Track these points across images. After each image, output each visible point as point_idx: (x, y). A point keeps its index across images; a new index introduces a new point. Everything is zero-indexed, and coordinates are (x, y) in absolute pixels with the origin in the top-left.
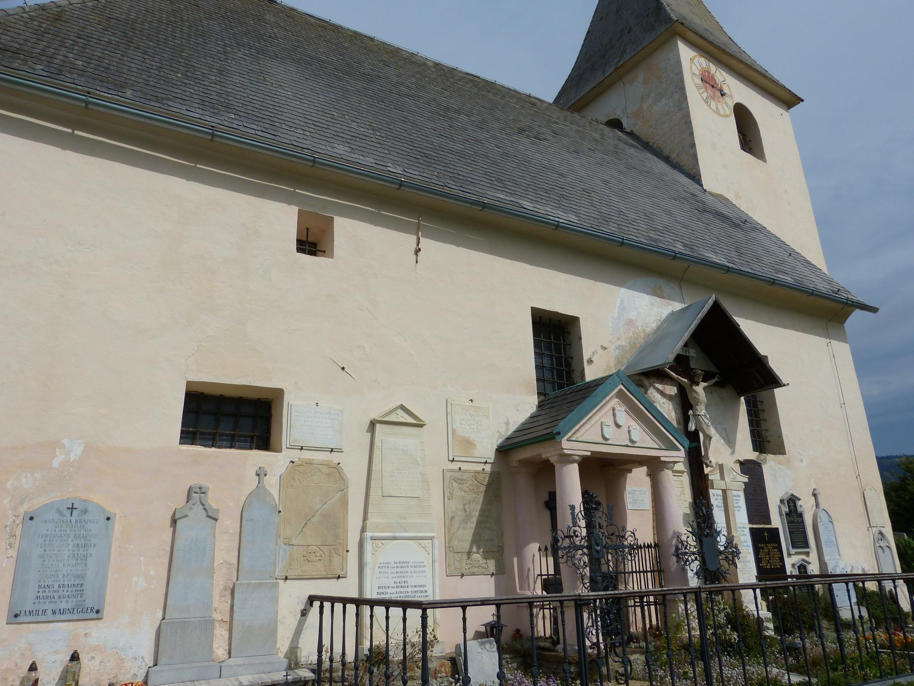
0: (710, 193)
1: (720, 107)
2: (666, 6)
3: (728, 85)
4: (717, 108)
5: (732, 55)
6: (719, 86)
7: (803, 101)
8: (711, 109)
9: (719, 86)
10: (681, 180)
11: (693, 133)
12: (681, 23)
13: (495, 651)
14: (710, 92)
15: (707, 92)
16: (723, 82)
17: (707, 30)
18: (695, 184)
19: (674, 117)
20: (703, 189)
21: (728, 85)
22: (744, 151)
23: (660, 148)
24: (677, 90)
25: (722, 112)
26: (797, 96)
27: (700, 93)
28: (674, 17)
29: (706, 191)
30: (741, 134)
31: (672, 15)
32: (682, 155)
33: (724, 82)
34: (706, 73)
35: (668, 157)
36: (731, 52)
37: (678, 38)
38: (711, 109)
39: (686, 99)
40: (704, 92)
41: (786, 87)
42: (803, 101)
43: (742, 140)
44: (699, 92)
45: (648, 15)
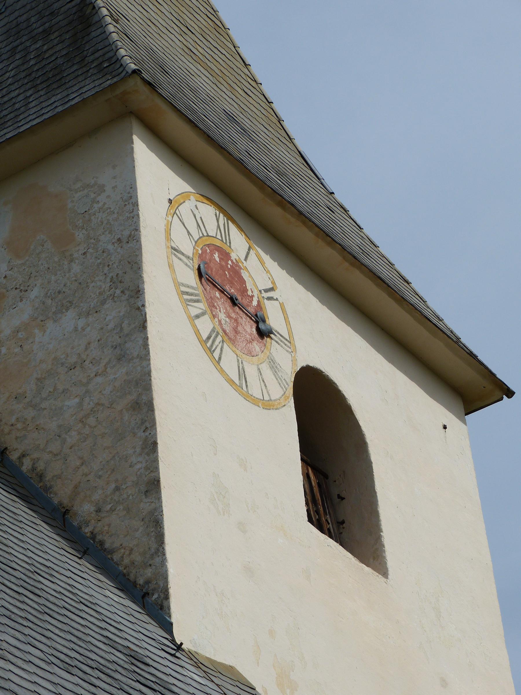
0: (192, 656)
1: (251, 371)
2: (108, 19)
3: (282, 306)
4: (242, 373)
5: (301, 213)
6: (255, 303)
7: (510, 394)
8: (222, 371)
9: (255, 303)
10: (99, 599)
11: (155, 444)
12: (150, 84)
13: (199, 236)
14: (222, 316)
15: (214, 316)
16: (266, 291)
17: (232, 118)
18: (145, 618)
19: (99, 379)
20: (173, 641)
21: (282, 306)
22: (321, 528)
23: (41, 476)
24: (118, 292)
25: (256, 391)
26: (494, 375)
27: (189, 317)
28: (127, 60)
29: (179, 647)
30: (314, 469)
31: (122, 52)
32: (112, 510)
33: (270, 294)
34: (216, 256)
35: (67, 512)
36: (300, 204)
37: (136, 126)
38: (222, 371)
39: (143, 326)
40: (203, 314)
41: (463, 340)
42: (510, 394)
43: (316, 490)
44: (187, 312)
45: (47, 33)
